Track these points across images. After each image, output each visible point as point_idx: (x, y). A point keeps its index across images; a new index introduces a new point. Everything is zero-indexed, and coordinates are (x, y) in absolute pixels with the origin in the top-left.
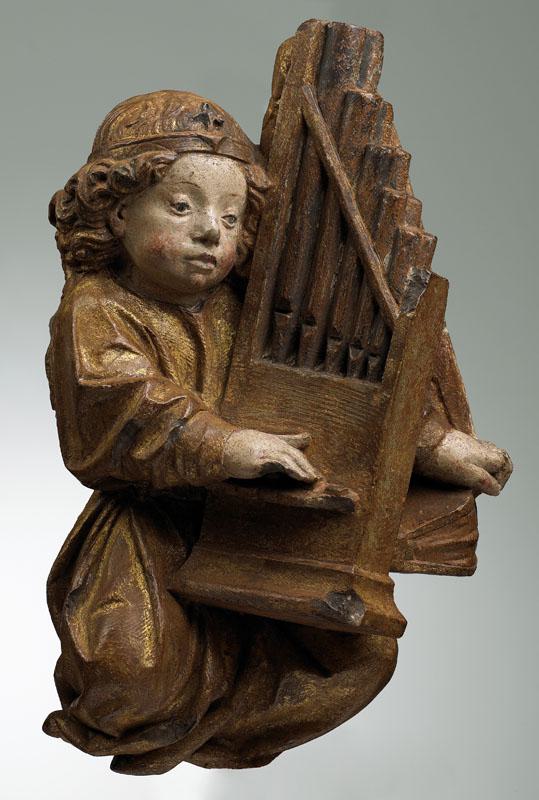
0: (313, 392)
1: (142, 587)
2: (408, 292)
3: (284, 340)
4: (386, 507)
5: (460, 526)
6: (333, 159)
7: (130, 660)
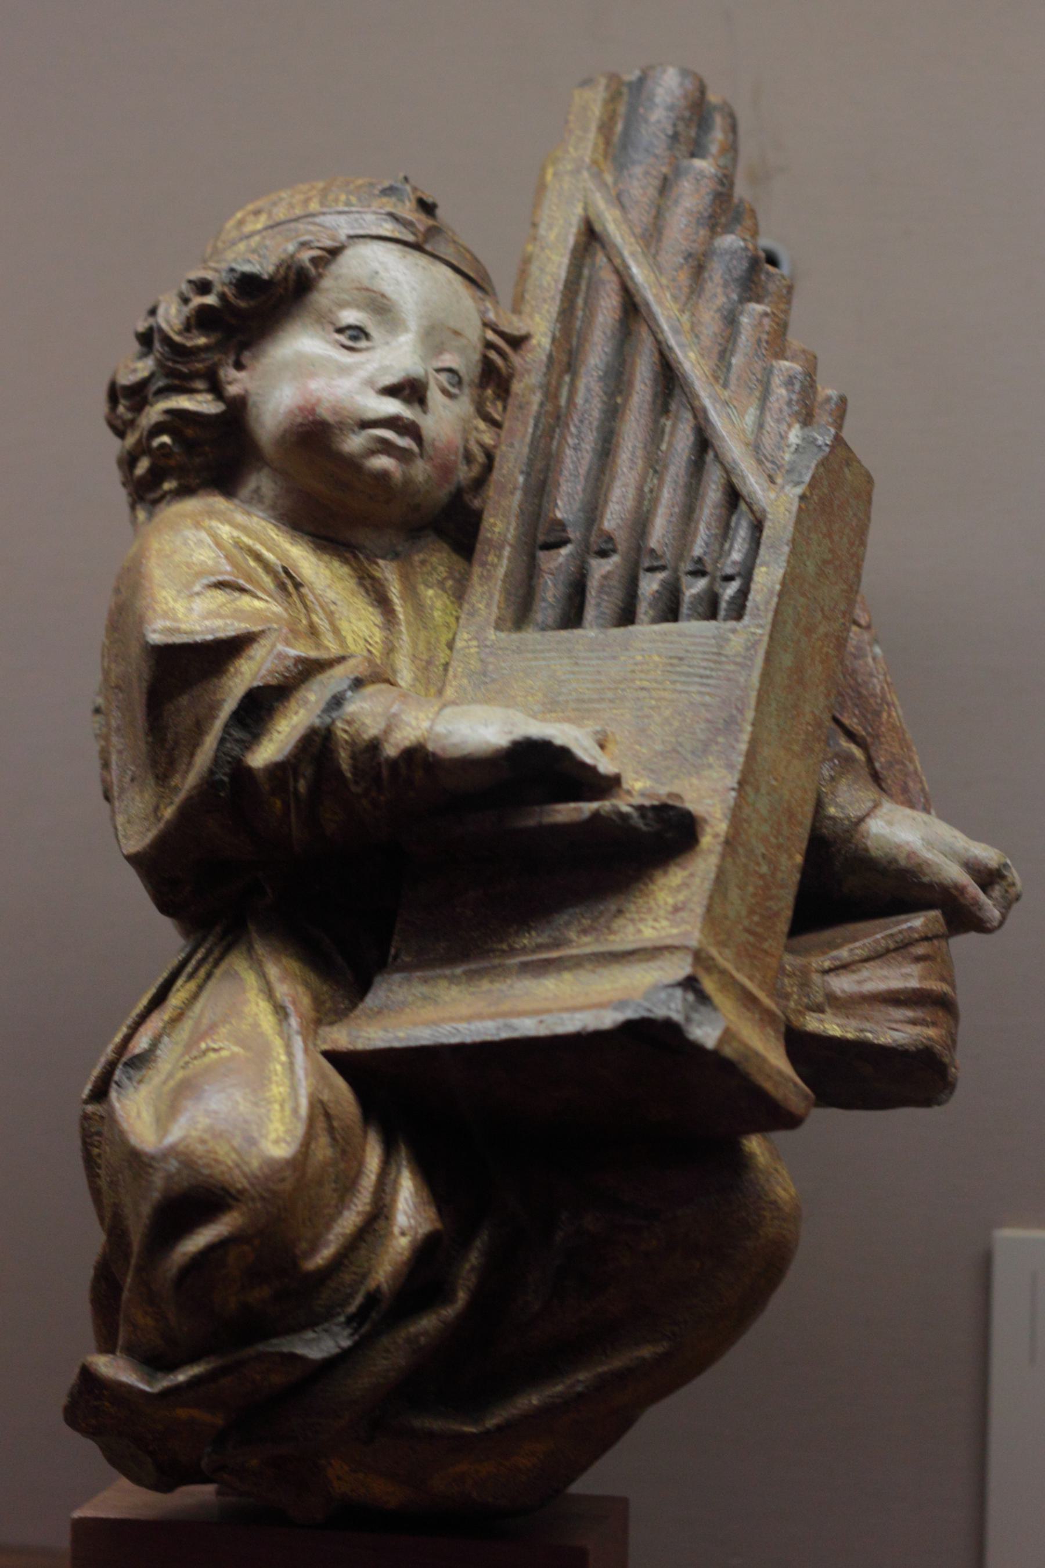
0: (614, 658)
2: (792, 463)
3: (551, 592)
4: (763, 850)
5: (918, 959)
6: (639, 273)
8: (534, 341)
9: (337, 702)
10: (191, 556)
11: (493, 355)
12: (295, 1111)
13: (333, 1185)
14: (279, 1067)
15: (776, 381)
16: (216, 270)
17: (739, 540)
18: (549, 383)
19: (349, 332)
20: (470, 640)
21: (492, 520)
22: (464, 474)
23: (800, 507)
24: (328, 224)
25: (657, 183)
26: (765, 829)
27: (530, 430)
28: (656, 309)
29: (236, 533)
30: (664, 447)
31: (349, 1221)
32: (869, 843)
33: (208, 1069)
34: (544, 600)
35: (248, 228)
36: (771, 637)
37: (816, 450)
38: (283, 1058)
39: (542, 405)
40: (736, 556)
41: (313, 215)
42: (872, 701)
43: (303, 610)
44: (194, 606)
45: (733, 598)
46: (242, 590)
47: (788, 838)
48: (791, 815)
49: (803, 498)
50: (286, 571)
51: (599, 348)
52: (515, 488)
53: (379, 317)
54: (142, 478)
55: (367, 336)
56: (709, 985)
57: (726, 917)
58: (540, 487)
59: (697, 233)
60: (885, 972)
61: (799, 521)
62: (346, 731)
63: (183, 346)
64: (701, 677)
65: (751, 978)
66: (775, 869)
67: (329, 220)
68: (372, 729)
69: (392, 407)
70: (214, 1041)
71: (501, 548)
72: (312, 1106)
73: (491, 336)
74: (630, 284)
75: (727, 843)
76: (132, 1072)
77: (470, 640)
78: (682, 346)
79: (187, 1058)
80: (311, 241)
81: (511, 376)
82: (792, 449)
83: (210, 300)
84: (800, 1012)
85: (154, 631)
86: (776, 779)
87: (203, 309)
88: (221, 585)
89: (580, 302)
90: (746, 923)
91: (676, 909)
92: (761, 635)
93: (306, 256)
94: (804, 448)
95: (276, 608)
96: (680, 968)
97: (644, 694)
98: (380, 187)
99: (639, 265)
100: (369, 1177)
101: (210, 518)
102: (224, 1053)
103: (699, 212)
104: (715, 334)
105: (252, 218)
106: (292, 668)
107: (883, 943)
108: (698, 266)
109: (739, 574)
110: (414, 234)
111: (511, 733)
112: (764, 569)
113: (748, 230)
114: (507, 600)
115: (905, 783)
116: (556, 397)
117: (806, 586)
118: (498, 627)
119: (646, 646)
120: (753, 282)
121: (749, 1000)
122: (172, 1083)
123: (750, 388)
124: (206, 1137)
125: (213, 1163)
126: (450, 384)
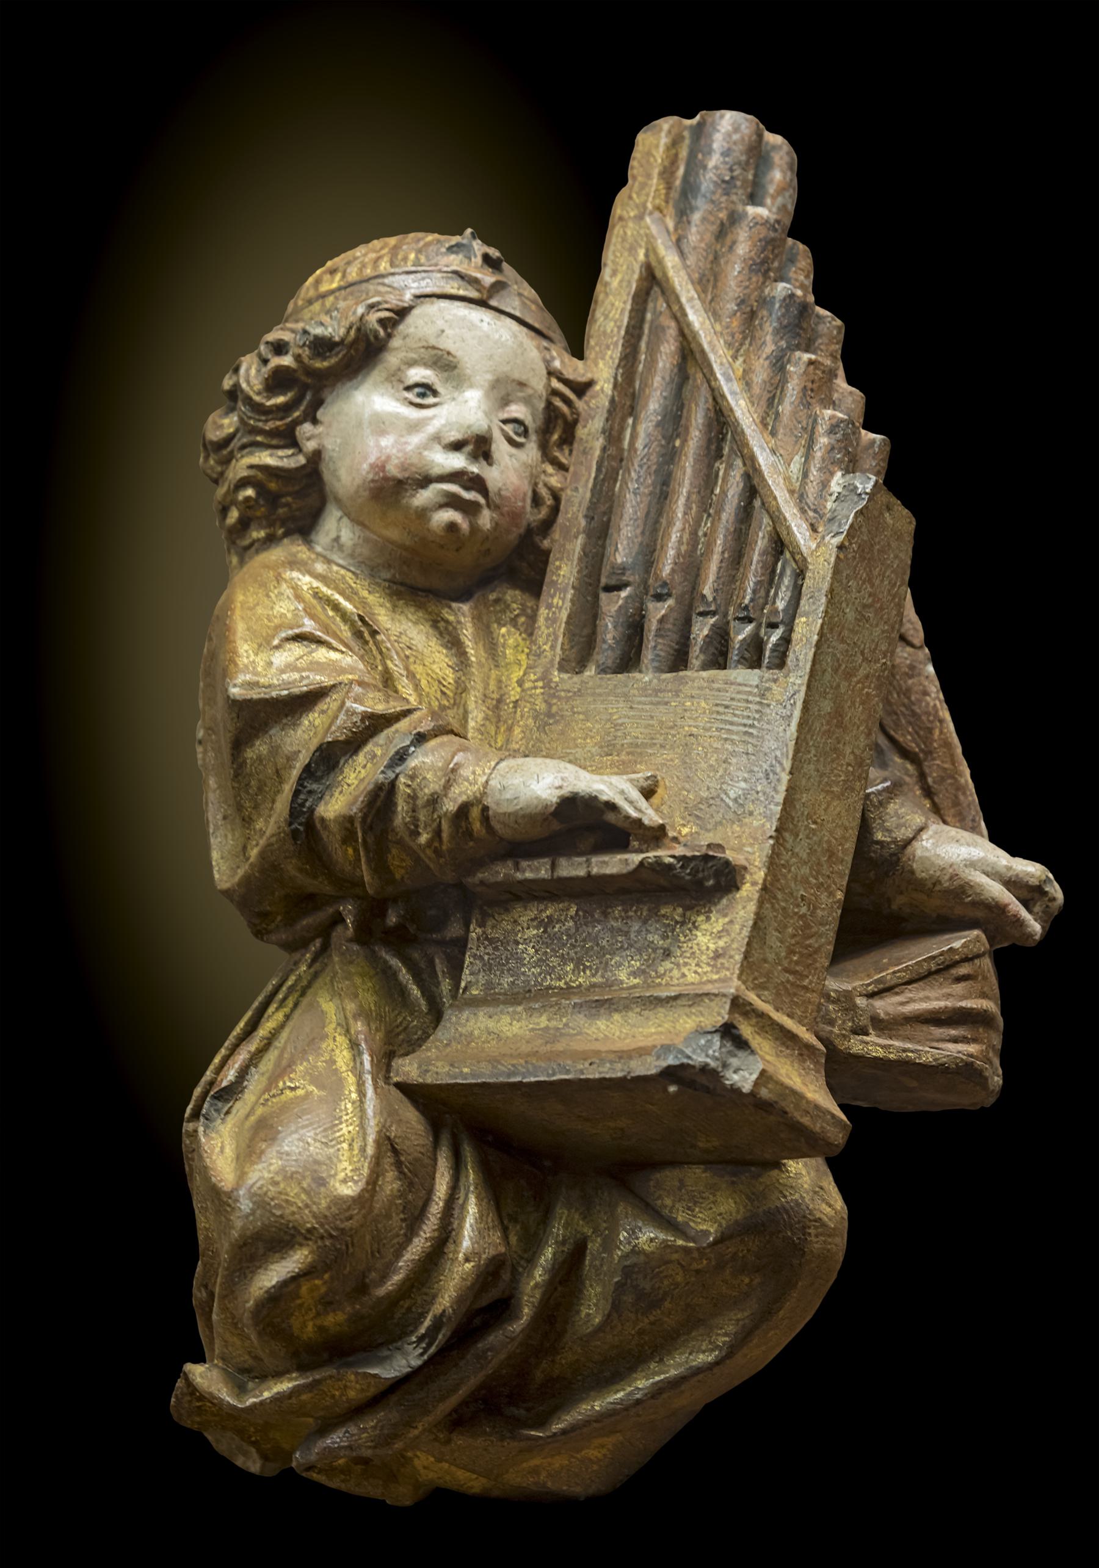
1: (344, 1068)
3: (610, 631)
5: (959, 979)
6: (696, 317)
7: (309, 1180)
8: (598, 388)
9: (401, 757)
10: (272, 608)
11: (558, 402)
12: (363, 1150)
13: (402, 1216)
14: (349, 1106)
15: (821, 429)
16: (293, 331)
17: (784, 589)
18: (611, 429)
19: (417, 390)
20: (536, 681)
21: (557, 563)
22: (535, 517)
23: (838, 557)
24: (395, 285)
25: (714, 228)
26: (805, 870)
27: (593, 475)
28: (712, 357)
29: (316, 584)
30: (717, 491)
31: (418, 1247)
32: (915, 866)
33: (285, 1108)
34: (604, 641)
35: (324, 288)
36: (809, 687)
37: (856, 498)
38: (354, 1096)
39: (604, 449)
40: (781, 605)
41: (382, 276)
42: (924, 718)
43: (379, 657)
44: (273, 659)
45: (776, 645)
46: (320, 642)
47: (828, 877)
48: (831, 854)
49: (841, 547)
50: (361, 618)
51: (658, 393)
52: (578, 533)
53: (446, 374)
54: (234, 526)
55: (435, 393)
56: (746, 1030)
57: (765, 961)
58: (600, 531)
59: (750, 279)
60: (927, 993)
61: (836, 571)
62: (409, 786)
63: (262, 405)
64: (745, 725)
65: (790, 1016)
66: (814, 908)
67: (398, 281)
68: (433, 784)
69: (457, 461)
70: (291, 1080)
71: (565, 591)
72: (378, 1143)
73: (556, 384)
74: (686, 331)
75: (764, 888)
76: (220, 1104)
77: (536, 681)
78: (733, 393)
79: (266, 1096)
80: (379, 303)
81: (576, 422)
82: (834, 498)
83: (287, 361)
84: (844, 1036)
85: (235, 686)
86: (815, 822)
87: (279, 371)
88: (299, 638)
89: (643, 345)
90: (786, 963)
91: (717, 955)
92: (800, 685)
93: (373, 318)
94: (845, 496)
95: (349, 660)
96: (719, 1014)
97: (693, 740)
98: (447, 245)
99: (696, 312)
100: (437, 1204)
101: (292, 570)
102: (300, 1092)
103: (751, 259)
104: (765, 382)
105: (327, 277)
106: (359, 724)
107: (925, 965)
108: (750, 316)
109: (782, 622)
110: (478, 290)
111: (560, 787)
112: (804, 619)
113: (803, 270)
114: (571, 641)
115: (956, 797)
116: (619, 439)
117: (846, 633)
118: (561, 669)
119: (694, 692)
120: (801, 328)
121: (786, 1038)
122: (252, 1118)
123: (796, 436)
124: (278, 1178)
125: (284, 1204)
126: (517, 434)
